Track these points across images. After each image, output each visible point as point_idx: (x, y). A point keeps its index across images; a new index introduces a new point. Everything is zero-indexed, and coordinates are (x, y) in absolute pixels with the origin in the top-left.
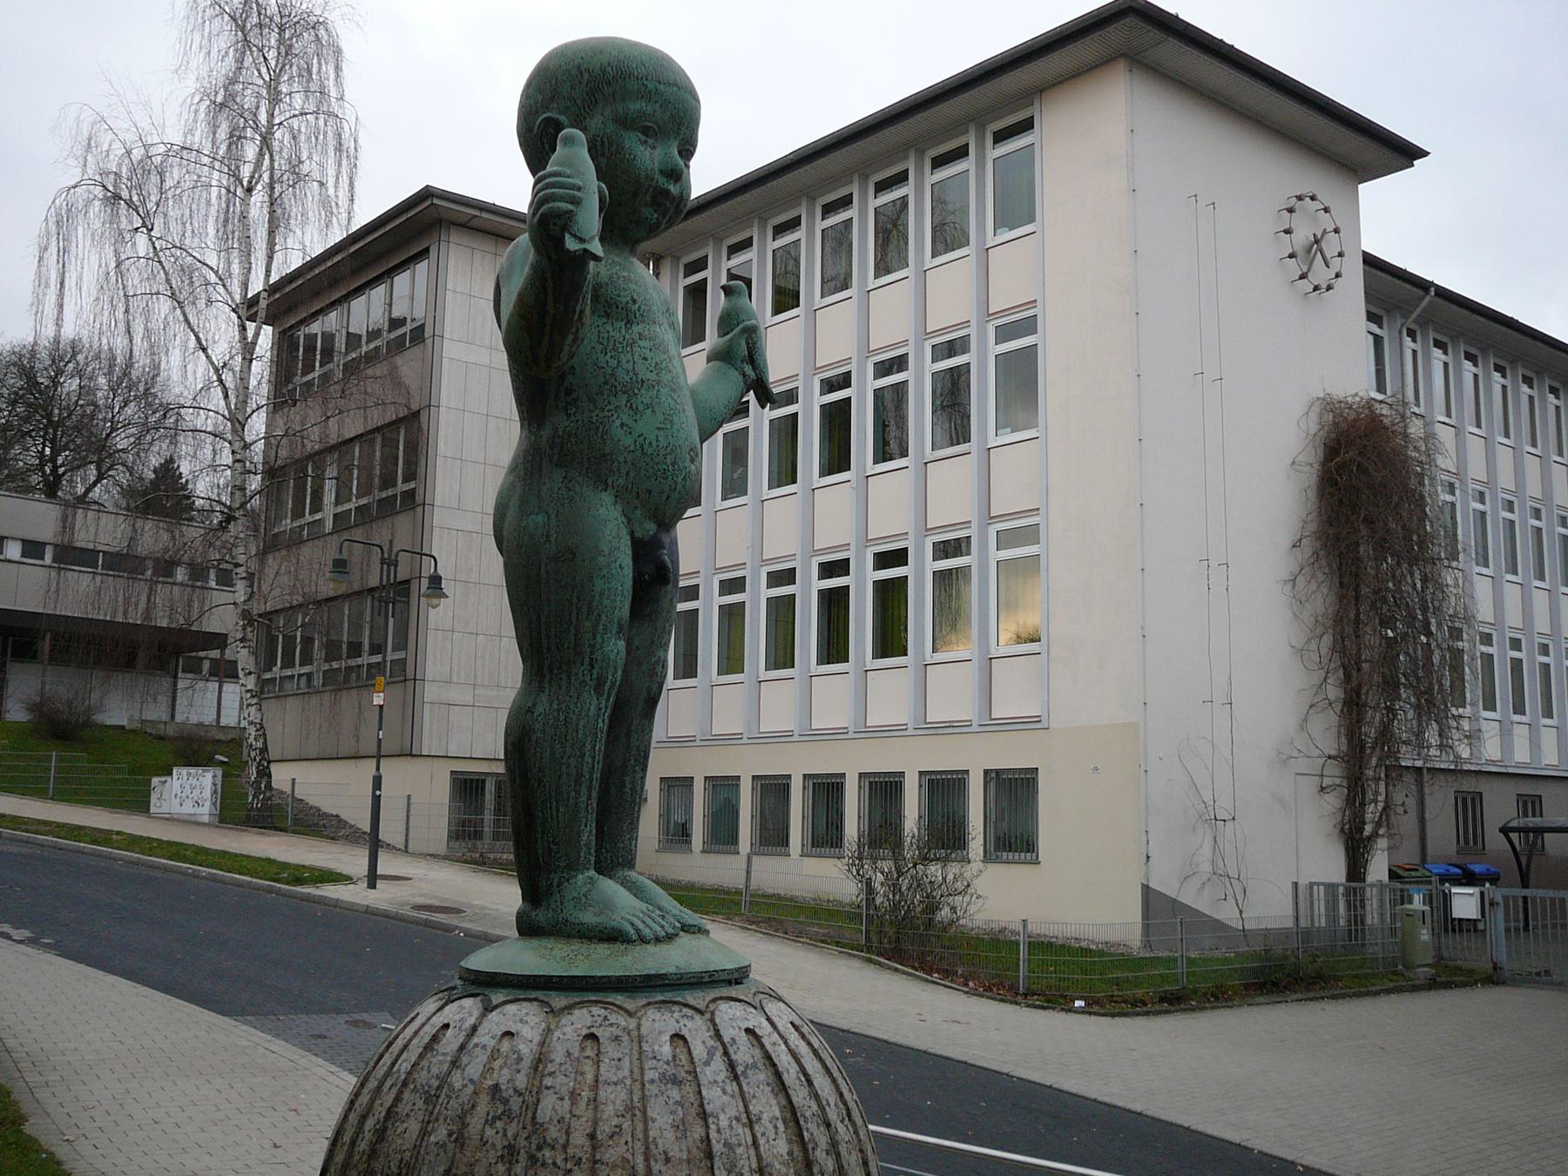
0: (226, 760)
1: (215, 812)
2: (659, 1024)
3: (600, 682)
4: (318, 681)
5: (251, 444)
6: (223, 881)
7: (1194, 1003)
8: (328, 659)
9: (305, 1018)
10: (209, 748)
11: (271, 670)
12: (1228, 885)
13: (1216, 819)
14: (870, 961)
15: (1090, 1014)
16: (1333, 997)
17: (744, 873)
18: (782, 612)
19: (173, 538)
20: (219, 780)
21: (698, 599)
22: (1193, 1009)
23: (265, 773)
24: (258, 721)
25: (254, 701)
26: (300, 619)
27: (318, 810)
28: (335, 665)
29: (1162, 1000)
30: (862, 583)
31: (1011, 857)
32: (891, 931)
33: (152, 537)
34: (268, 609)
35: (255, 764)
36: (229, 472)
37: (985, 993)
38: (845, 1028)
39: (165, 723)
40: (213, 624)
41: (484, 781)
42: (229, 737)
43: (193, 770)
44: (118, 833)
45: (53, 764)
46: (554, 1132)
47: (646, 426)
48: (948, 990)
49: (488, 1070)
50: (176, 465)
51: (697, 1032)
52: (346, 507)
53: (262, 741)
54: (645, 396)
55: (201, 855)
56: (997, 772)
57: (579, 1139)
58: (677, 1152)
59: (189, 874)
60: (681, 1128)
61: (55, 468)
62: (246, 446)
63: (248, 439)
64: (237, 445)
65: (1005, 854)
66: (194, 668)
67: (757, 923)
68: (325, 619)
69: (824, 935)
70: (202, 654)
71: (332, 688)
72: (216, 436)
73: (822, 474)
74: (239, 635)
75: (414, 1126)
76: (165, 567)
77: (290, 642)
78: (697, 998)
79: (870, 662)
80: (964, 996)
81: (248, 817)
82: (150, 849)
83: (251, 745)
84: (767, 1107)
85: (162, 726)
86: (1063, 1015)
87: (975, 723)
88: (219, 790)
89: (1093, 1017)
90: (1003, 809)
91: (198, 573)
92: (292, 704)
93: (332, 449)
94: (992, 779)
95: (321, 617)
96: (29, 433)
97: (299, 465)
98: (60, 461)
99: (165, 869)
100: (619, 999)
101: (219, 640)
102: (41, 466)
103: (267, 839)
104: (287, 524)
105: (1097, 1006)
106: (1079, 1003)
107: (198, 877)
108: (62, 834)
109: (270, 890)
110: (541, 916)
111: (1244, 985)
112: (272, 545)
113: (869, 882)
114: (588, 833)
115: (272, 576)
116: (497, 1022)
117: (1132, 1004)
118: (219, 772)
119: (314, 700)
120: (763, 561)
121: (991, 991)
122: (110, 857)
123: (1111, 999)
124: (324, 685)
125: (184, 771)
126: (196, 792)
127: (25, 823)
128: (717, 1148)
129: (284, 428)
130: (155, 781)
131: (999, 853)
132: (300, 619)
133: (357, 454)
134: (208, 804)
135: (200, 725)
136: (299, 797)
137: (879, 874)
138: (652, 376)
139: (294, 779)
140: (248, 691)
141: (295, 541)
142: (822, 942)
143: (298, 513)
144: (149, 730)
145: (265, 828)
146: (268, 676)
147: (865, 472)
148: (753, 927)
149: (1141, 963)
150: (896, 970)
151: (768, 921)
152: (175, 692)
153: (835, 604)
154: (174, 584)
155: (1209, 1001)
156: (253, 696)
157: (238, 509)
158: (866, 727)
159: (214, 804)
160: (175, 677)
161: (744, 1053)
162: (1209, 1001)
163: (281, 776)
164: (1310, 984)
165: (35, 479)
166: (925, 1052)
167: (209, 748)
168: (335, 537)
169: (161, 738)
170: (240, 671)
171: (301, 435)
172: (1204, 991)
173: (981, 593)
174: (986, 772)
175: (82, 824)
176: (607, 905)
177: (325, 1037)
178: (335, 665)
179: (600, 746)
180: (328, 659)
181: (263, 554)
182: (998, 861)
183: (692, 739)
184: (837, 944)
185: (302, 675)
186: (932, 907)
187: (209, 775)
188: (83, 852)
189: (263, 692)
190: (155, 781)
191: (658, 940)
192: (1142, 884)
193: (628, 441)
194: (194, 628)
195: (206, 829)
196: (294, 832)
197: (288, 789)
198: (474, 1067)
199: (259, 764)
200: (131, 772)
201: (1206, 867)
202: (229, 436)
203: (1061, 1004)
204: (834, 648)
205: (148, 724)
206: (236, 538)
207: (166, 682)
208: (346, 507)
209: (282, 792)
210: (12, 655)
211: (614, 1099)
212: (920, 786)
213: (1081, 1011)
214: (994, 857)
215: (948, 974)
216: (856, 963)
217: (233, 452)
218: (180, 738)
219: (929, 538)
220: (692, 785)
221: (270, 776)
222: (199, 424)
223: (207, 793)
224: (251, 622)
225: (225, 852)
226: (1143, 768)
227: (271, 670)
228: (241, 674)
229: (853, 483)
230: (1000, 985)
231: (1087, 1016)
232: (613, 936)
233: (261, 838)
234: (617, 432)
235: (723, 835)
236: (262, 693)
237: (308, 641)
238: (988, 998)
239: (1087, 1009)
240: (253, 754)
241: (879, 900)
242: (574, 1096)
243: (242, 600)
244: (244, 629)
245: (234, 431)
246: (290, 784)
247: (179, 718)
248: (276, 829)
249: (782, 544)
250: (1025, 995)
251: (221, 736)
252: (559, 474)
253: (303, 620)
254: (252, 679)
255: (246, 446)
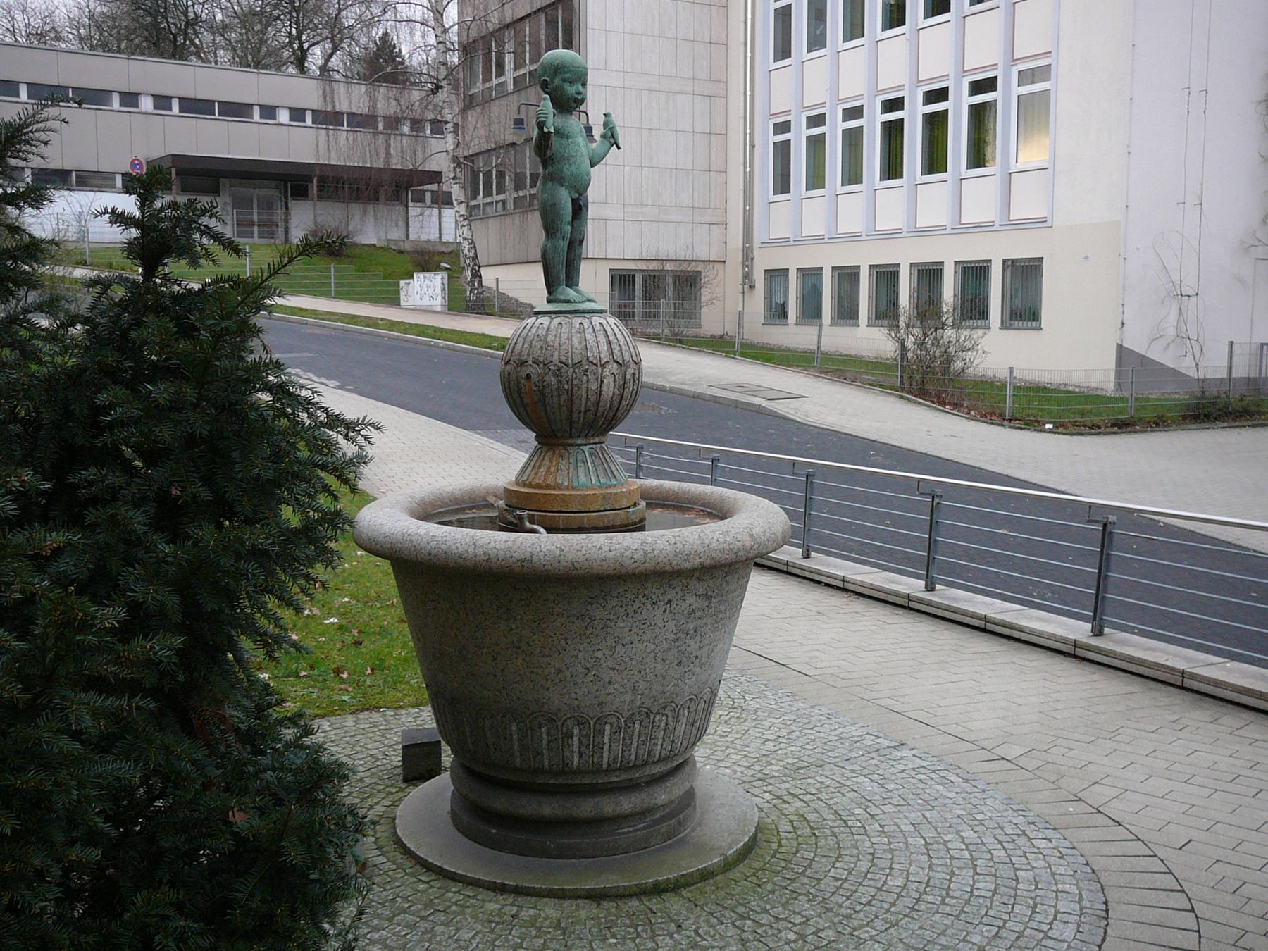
0: (449, 266)
1: (444, 304)
2: (576, 321)
3: (564, 237)
4: (510, 205)
5: (449, 29)
6: (454, 350)
7: (1138, 428)
8: (517, 188)
9: (513, 431)
10: (436, 258)
11: (475, 199)
12: (1189, 345)
13: (1181, 295)
14: (901, 397)
15: (1055, 433)
16: (1254, 426)
17: (816, 337)
18: (853, 139)
19: (399, 104)
20: (446, 281)
21: (790, 131)
22: (1136, 432)
23: (477, 275)
24: (470, 237)
25: (466, 223)
26: (494, 160)
27: (516, 300)
28: (521, 193)
29: (1113, 425)
30: (914, 117)
31: (1034, 325)
32: (918, 377)
33: (385, 101)
34: (471, 153)
35: (470, 268)
36: (434, 51)
37: (982, 419)
38: (874, 439)
39: (404, 241)
40: (432, 166)
41: (634, 276)
42: (449, 250)
43: (427, 274)
44: (382, 319)
45: (332, 273)
46: (551, 344)
47: (573, 169)
48: (954, 416)
49: (537, 331)
50: (390, 38)
51: (586, 323)
52: (522, 72)
53: (473, 252)
54: (572, 160)
55: (439, 333)
56: (1013, 261)
57: (556, 344)
58: (579, 347)
59: (432, 346)
60: (580, 343)
61: (301, 44)
62: (445, 31)
63: (447, 26)
64: (439, 31)
65: (1016, 323)
66: (420, 199)
67: (826, 373)
68: (512, 160)
69: (874, 380)
70: (425, 187)
71: (520, 210)
72: (422, 24)
73: (884, 29)
74: (452, 175)
75: (521, 345)
76: (393, 123)
77: (488, 175)
78: (588, 316)
79: (920, 178)
80: (965, 421)
81: (468, 307)
82: (405, 330)
83: (466, 255)
84: (602, 339)
85: (402, 243)
86: (1035, 434)
87: (949, 227)
88: (446, 288)
89: (1057, 435)
90: (1017, 290)
91: (416, 124)
92: (492, 223)
93: (508, 26)
94: (1008, 266)
95: (509, 160)
96: (278, 18)
97: (486, 39)
98: (304, 37)
99: (416, 342)
100: (568, 315)
101: (436, 177)
102: (290, 44)
103: (481, 321)
104: (478, 88)
105: (1063, 428)
106: (1049, 426)
107: (438, 347)
108: (346, 320)
109: (487, 355)
110: (552, 297)
111: (1181, 416)
112: (469, 103)
113: (902, 343)
114: (563, 276)
115: (472, 129)
116: (539, 321)
117: (1089, 428)
118: (446, 275)
119: (508, 220)
120: (839, 100)
121: (986, 417)
122: (379, 336)
123: (1074, 424)
124: (514, 209)
125: (421, 275)
126: (431, 291)
127: (321, 314)
128: (588, 347)
129: (472, 16)
130: (402, 283)
131: (1012, 322)
132: (494, 160)
133: (527, 32)
134: (439, 298)
135: (429, 241)
136: (502, 292)
137: (910, 336)
138: (574, 154)
139: (497, 279)
140: (461, 216)
141: (487, 101)
142: (870, 385)
143: (487, 78)
144: (393, 247)
145: (480, 314)
146: (474, 203)
147: (917, 26)
148: (823, 375)
149: (1116, 400)
150: (920, 403)
151: (834, 372)
152: (407, 219)
153: (936, 125)
154: (402, 135)
155: (1151, 427)
156: (464, 220)
157: (443, 79)
158: (916, 228)
159: (444, 298)
160: (407, 206)
161: (598, 327)
162: (1151, 427)
163: (488, 276)
164: (1237, 417)
165: (286, 54)
166: (925, 454)
167: (436, 258)
168: (516, 95)
169: (401, 252)
170: (454, 201)
171: (485, 19)
172: (1148, 419)
173: (1005, 123)
174: (1005, 261)
175: (357, 314)
176: (568, 294)
177: (527, 442)
178: (521, 193)
179: (565, 254)
180: (517, 188)
181: (464, 110)
182: (1011, 327)
183: (787, 240)
184: (881, 386)
185: (499, 201)
186: (949, 360)
187: (439, 278)
188: (361, 333)
189: (472, 214)
190: (402, 283)
191: (580, 302)
192: (1117, 344)
193: (569, 173)
194: (420, 169)
195: (439, 316)
196: (501, 316)
197: (493, 286)
198: (533, 331)
199: (473, 268)
200: (385, 278)
201: (1171, 332)
202: (432, 23)
203: (1034, 426)
204: (935, 161)
205: (392, 242)
206: (444, 102)
207: (399, 209)
208: (522, 72)
209: (489, 288)
210: (291, 196)
211: (564, 336)
212: (955, 272)
213: (1050, 431)
214: (1008, 325)
215: (956, 406)
216: (892, 399)
217: (436, 36)
218: (415, 252)
219: (965, 78)
220: (787, 275)
221: (481, 277)
222: (411, 15)
223: (439, 291)
224: (459, 165)
225: (453, 330)
226: (1122, 257)
227: (475, 199)
228: (455, 203)
229: (907, 35)
230: (991, 414)
231: (1052, 435)
232: (568, 302)
233: (477, 321)
234: (565, 170)
235: (811, 312)
236: (471, 216)
237: (501, 175)
238: (983, 422)
239: (1054, 430)
240: (468, 261)
241: (910, 355)
242: (556, 336)
243: (452, 148)
244: (455, 170)
245: (436, 20)
246: (495, 281)
247: (412, 237)
248: (487, 314)
249: (854, 87)
250: (1010, 420)
251: (444, 249)
252: (551, 183)
253: (496, 161)
254: (463, 206)
255: (445, 31)
